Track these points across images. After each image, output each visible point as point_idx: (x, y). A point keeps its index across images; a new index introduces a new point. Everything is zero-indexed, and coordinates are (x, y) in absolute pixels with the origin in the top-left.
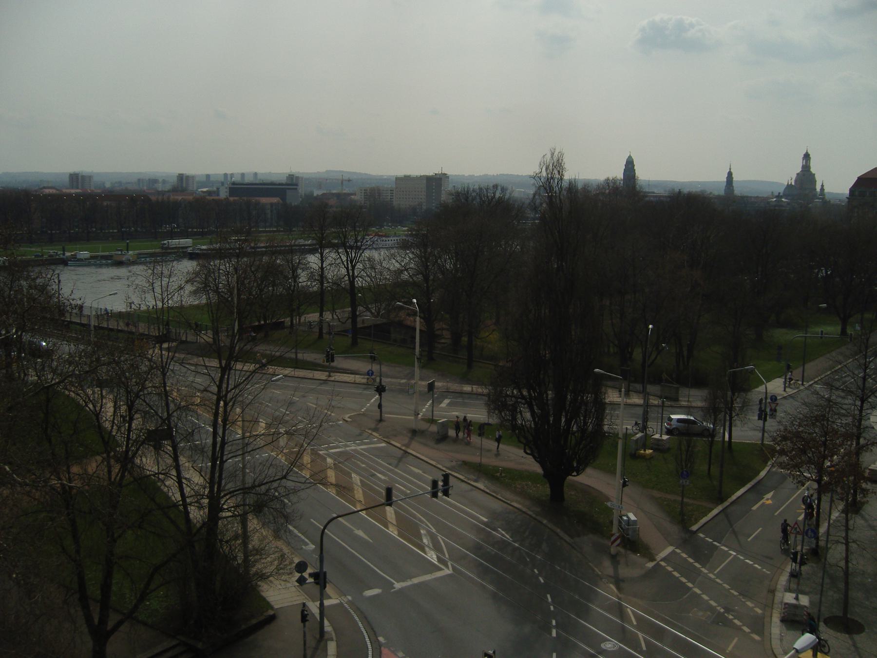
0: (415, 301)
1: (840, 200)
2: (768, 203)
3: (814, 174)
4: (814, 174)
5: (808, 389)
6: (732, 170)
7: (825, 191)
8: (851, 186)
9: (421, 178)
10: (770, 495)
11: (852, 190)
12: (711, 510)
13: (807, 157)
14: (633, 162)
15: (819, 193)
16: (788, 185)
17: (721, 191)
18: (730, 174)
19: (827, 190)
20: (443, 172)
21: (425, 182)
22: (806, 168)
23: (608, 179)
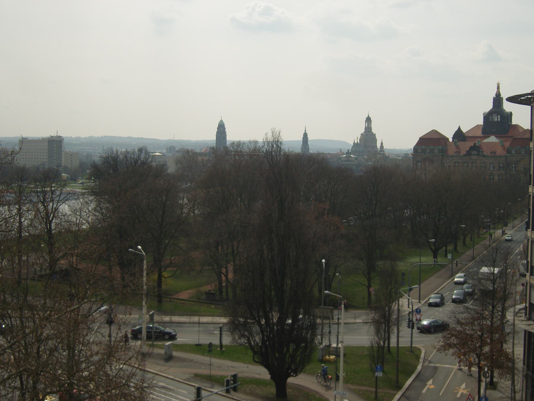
0: (140, 247)
1: (396, 155)
2: (340, 159)
3: (375, 134)
4: (375, 134)
5: (424, 305)
6: (307, 132)
7: (384, 148)
8: (415, 144)
9: (43, 140)
10: (430, 382)
11: (415, 149)
12: (395, 395)
13: (368, 120)
14: (224, 125)
15: (379, 150)
16: (354, 143)
17: (298, 149)
18: (305, 135)
19: (385, 147)
20: (58, 135)
21: (47, 144)
22: (368, 129)
23: (240, 141)
